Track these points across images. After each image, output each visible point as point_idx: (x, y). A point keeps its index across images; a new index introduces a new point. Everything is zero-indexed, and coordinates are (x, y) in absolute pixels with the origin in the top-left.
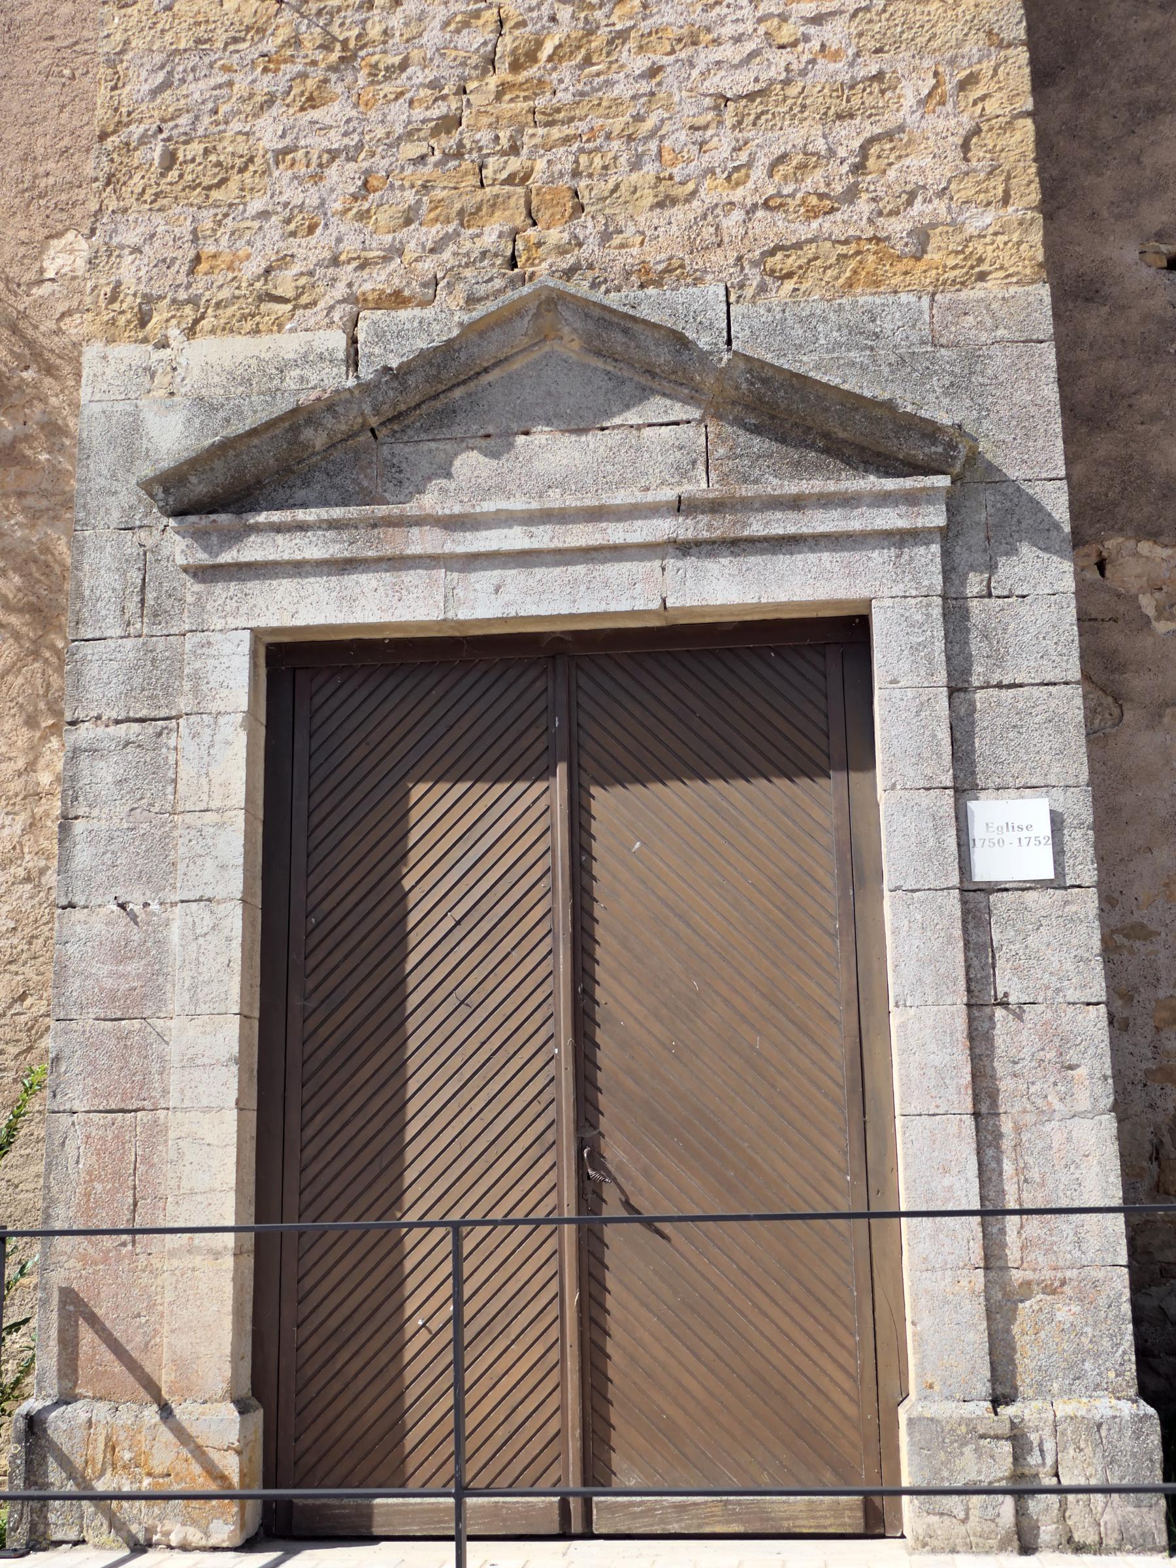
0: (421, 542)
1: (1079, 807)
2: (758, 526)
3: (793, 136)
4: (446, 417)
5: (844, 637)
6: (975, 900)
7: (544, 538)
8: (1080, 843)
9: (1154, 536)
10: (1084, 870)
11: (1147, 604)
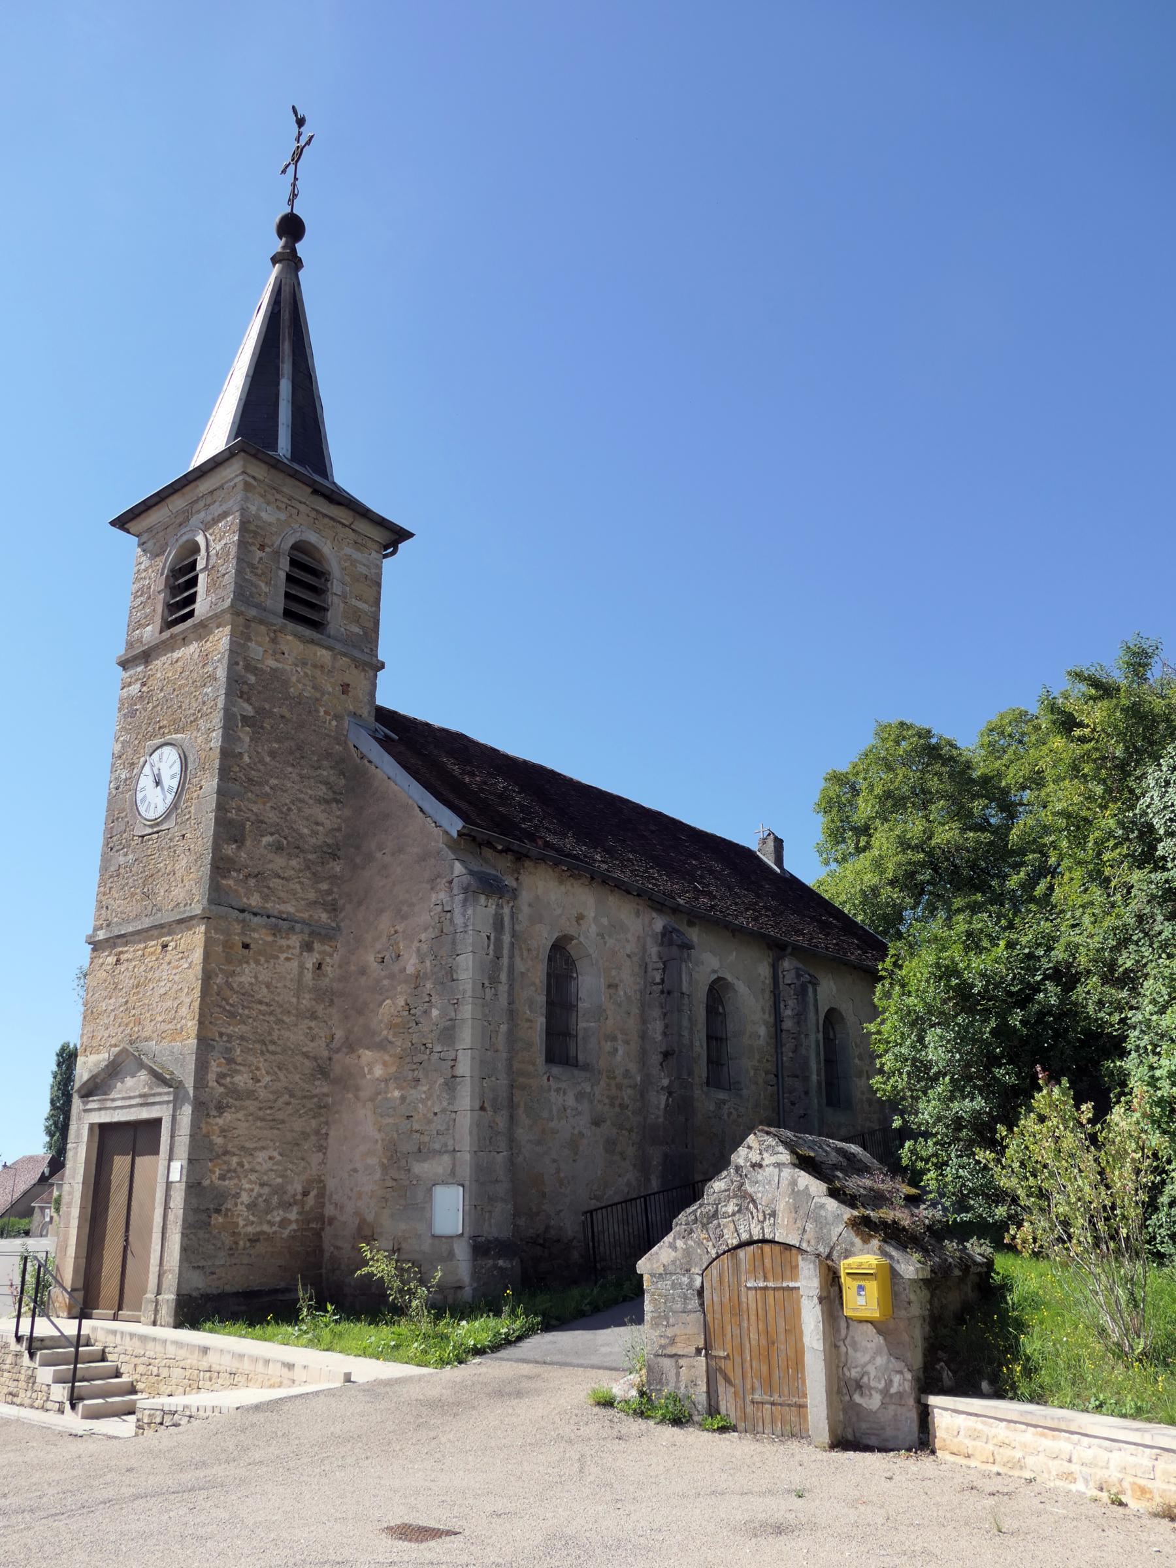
0: (109, 1104)
1: (185, 1163)
2: (151, 1100)
3: (169, 1003)
4: (117, 1074)
5: (157, 1122)
6: (169, 1184)
7: (128, 1103)
8: (185, 1172)
9: (368, 1048)
10: (184, 1179)
11: (366, 1069)
